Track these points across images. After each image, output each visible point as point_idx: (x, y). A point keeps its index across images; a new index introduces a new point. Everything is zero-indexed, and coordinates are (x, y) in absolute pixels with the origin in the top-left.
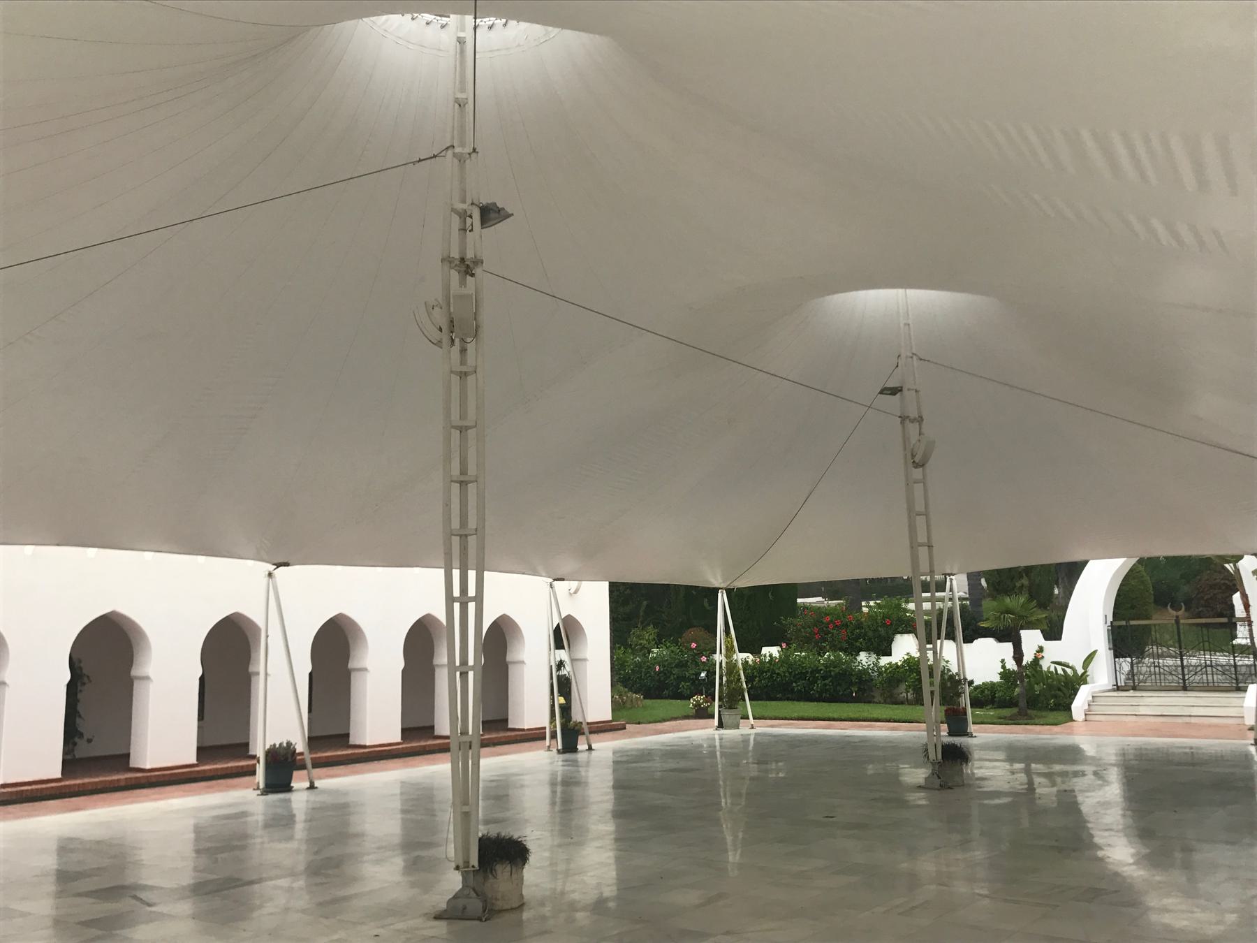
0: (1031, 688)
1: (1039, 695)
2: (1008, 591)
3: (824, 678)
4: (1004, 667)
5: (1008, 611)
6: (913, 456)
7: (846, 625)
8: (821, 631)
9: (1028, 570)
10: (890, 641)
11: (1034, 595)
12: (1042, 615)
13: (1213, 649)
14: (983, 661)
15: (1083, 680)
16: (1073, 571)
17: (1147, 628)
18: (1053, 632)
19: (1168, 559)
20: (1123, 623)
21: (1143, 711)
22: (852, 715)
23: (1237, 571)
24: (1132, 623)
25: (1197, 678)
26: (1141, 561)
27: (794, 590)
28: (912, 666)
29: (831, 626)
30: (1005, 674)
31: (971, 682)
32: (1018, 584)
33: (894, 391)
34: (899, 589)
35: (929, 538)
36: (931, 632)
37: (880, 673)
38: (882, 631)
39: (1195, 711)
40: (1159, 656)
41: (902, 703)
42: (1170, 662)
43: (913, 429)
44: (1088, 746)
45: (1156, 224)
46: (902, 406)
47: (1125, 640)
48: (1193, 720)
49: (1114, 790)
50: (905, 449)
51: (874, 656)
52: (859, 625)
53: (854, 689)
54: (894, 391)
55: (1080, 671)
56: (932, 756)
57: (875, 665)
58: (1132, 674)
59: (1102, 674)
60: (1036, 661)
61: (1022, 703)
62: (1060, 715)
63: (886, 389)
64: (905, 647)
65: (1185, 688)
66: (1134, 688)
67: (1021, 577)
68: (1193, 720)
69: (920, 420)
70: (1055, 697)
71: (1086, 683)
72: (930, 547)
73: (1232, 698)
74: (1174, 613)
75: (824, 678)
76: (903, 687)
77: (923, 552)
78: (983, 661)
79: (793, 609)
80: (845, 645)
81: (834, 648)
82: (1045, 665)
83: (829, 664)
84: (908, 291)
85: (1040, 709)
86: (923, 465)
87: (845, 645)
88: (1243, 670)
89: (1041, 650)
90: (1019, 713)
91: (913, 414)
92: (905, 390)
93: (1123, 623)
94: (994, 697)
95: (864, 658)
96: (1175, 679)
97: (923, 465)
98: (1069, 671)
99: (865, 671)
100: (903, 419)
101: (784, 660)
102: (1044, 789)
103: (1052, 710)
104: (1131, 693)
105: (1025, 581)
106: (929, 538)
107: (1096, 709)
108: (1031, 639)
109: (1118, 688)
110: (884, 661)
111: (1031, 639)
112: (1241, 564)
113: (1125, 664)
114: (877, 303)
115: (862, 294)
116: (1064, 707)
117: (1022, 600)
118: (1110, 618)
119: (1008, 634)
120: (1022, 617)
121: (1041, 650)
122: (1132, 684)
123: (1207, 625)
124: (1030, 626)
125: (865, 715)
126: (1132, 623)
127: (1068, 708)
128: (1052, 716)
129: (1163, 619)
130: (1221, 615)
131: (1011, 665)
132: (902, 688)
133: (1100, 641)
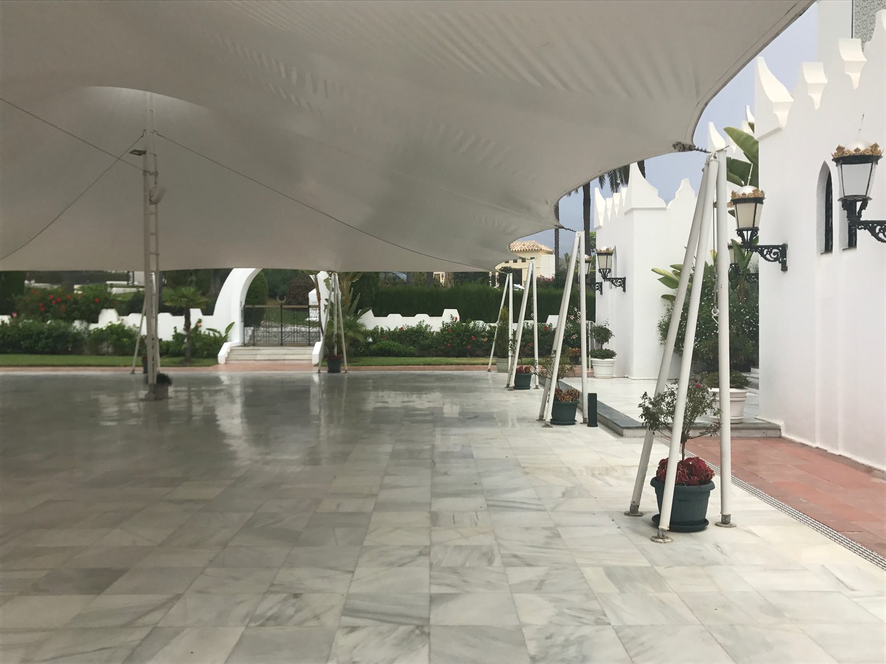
0: (193, 344)
1: (200, 348)
2: (184, 283)
3: (47, 338)
4: (175, 331)
5: (184, 296)
6: (151, 197)
7: (66, 302)
8: (44, 306)
9: (196, 271)
10: (98, 313)
11: (203, 287)
12: (204, 299)
13: (298, 325)
14: (168, 326)
15: (224, 339)
16: (223, 274)
17: (262, 311)
18: (209, 311)
19: (757, 308)
20: (251, 306)
21: (259, 357)
22: (55, 363)
23: (316, 279)
24: (257, 306)
25: (289, 339)
26: (263, 270)
27: (21, 276)
28: (112, 329)
29: (53, 302)
30: (177, 336)
31: (161, 340)
32: (189, 279)
33: (140, 153)
34: (101, 277)
35: (157, 250)
36: (128, 307)
37: (90, 335)
38: (93, 306)
39: (287, 357)
40: (269, 327)
41: (104, 355)
42: (275, 330)
43: (151, 179)
44: (224, 377)
45: (282, 69)
46: (145, 166)
47: (252, 315)
48: (286, 362)
49: (238, 408)
50: (145, 191)
51: (85, 324)
52: (76, 302)
53: (70, 345)
54: (140, 153)
55: (224, 335)
56: (150, 381)
57: (87, 328)
58: (253, 336)
59: (236, 337)
60: (197, 327)
61: (188, 354)
62: (211, 361)
63: (135, 151)
64: (108, 318)
65: (282, 345)
66: (254, 345)
67: (191, 275)
68: (286, 362)
69: (156, 174)
70: (207, 350)
71: (226, 341)
72: (157, 255)
73: (306, 350)
74: (280, 302)
75: (47, 338)
76: (105, 344)
77: (153, 258)
78: (168, 326)
79: (21, 289)
80: (64, 316)
81: (55, 317)
82: (203, 330)
83: (51, 329)
84: (154, 94)
85: (198, 357)
86: (156, 203)
87: (64, 316)
88: (313, 335)
89: (200, 321)
90: (186, 360)
91: (152, 170)
92: (148, 152)
93: (251, 306)
94: (168, 350)
95: (77, 324)
96: (277, 340)
97: (156, 203)
98: (217, 334)
99: (79, 333)
100: (145, 172)
101: (14, 325)
102: (197, 409)
103: (205, 358)
104: (251, 348)
105: (194, 278)
106: (157, 250)
107: (232, 357)
108: (196, 314)
109: (244, 345)
110: (93, 327)
111: (196, 314)
112: (319, 275)
113: (250, 330)
114: (128, 95)
115: (118, 90)
116: (213, 355)
117: (192, 290)
118: (243, 303)
119: (180, 310)
120: (192, 300)
121: (200, 321)
122: (251, 343)
123: (293, 309)
124: (195, 306)
125: (80, 363)
126: (257, 306)
127: (215, 356)
128: (206, 361)
129: (272, 305)
130: (301, 304)
131: (181, 330)
132: (121, 343)
133: (236, 317)
